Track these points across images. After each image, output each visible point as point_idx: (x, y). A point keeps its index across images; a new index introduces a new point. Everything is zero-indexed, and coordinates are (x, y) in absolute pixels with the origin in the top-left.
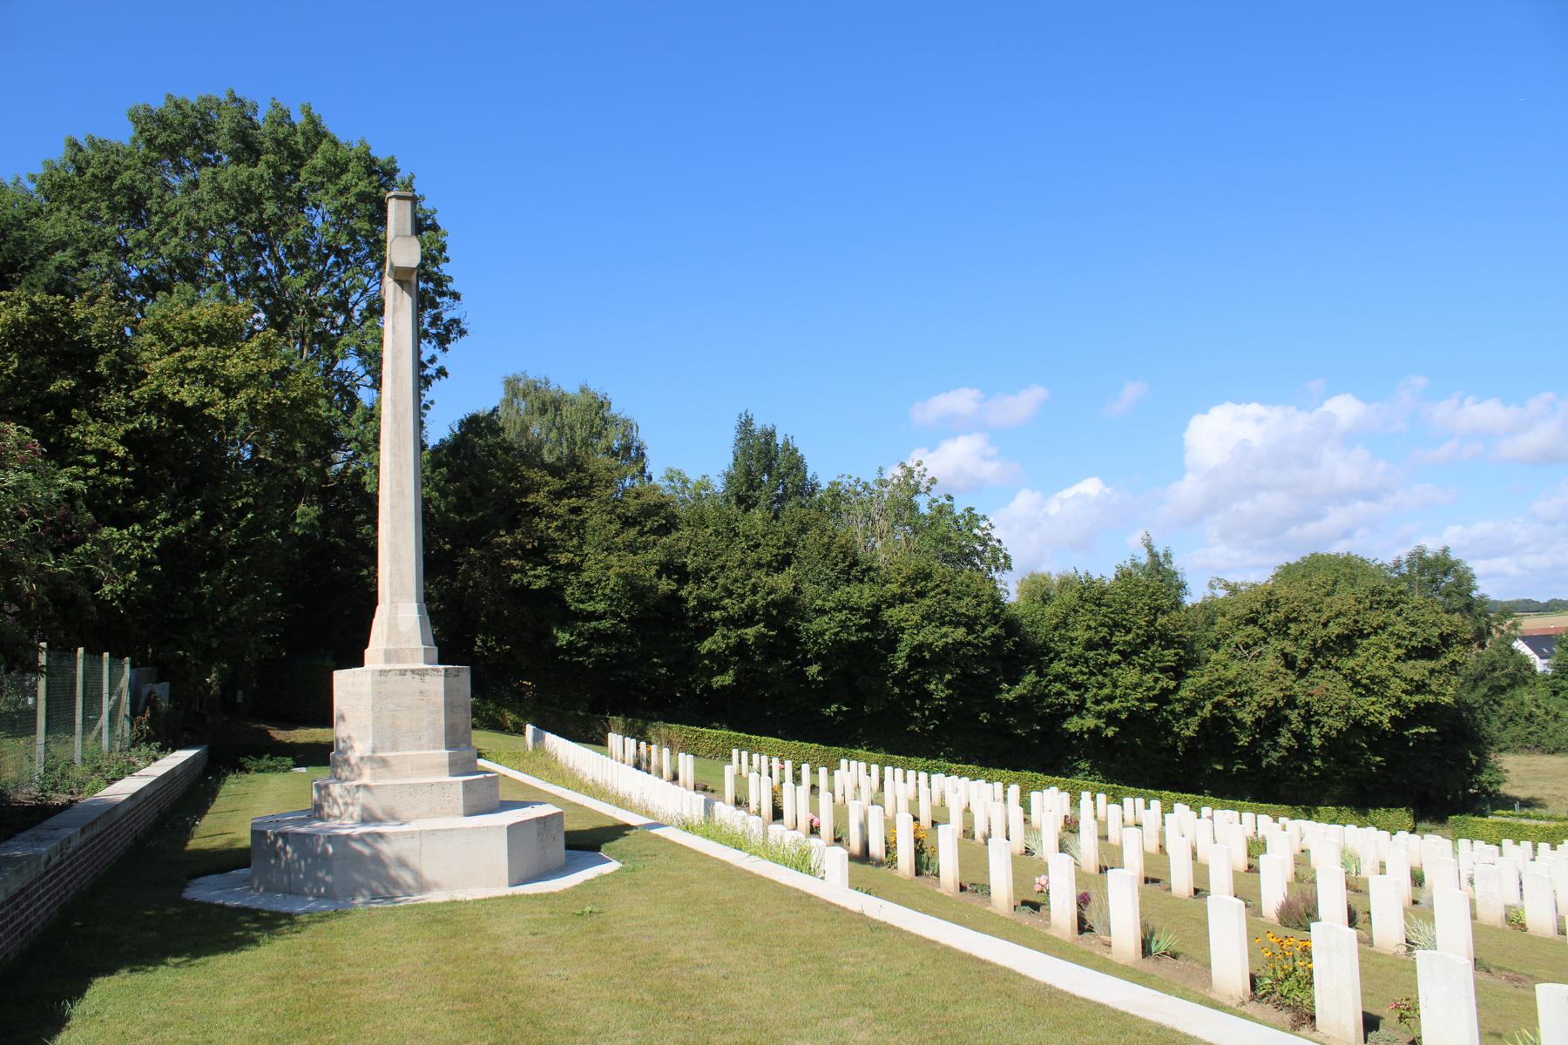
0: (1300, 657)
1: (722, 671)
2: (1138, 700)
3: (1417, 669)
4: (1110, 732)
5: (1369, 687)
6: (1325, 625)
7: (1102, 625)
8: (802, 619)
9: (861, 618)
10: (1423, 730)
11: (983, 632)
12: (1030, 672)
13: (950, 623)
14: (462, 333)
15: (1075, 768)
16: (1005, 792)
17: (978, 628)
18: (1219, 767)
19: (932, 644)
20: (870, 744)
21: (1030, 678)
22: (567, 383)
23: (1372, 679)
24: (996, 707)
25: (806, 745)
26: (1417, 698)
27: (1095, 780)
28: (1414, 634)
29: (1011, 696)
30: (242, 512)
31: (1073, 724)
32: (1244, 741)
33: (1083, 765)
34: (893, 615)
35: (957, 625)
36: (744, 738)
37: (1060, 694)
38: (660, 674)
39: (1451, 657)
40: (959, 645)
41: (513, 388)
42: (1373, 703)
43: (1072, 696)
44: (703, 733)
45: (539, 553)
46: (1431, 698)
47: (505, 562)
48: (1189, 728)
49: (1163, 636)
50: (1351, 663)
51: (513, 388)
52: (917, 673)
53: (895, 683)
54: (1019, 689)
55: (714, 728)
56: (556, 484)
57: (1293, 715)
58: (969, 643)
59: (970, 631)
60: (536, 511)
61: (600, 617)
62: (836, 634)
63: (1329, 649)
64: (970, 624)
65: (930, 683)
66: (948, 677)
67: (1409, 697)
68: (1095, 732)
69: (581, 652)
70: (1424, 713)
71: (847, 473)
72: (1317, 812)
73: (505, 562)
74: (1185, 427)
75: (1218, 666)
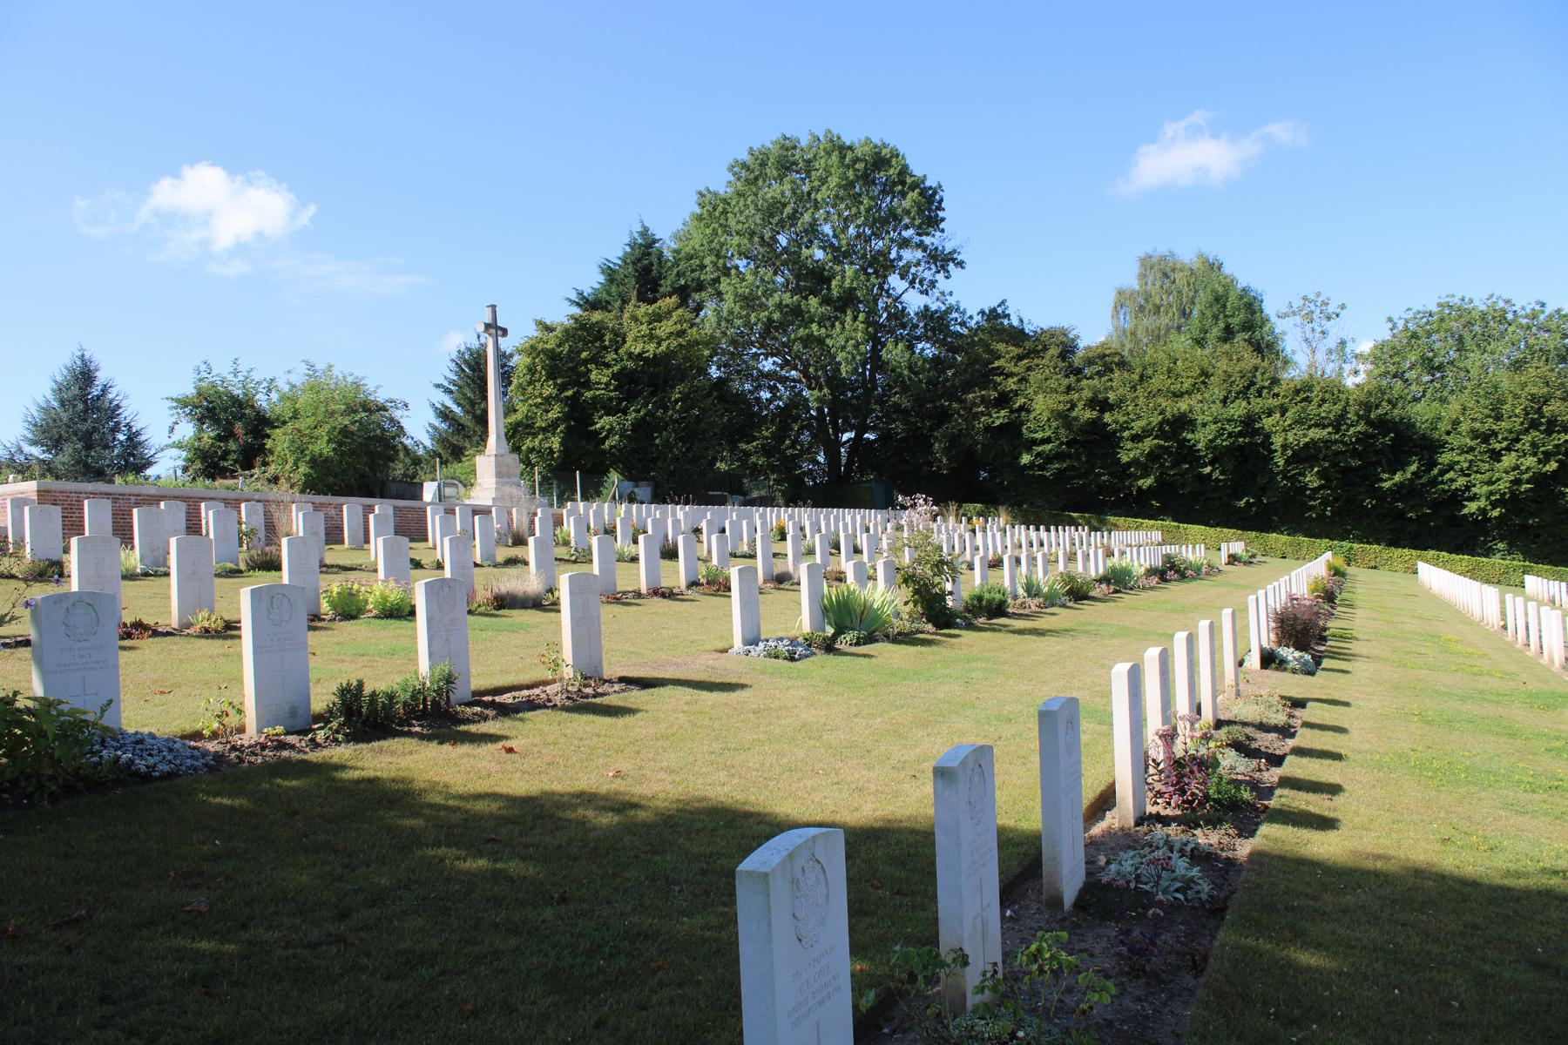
14: (960, 264)
22: (1187, 255)
25: (1225, 530)
27: (1514, 559)
30: (676, 401)
33: (1501, 546)
37: (1452, 480)
38: (1105, 481)
40: (1327, 443)
41: (1147, 264)
44: (1142, 523)
45: (1004, 400)
47: (975, 410)
51: (1147, 264)
54: (1398, 477)
56: (1015, 351)
59: (1337, 431)
60: (1000, 371)
61: (1047, 441)
64: (1338, 423)
68: (1483, 511)
69: (1041, 467)
73: (975, 410)
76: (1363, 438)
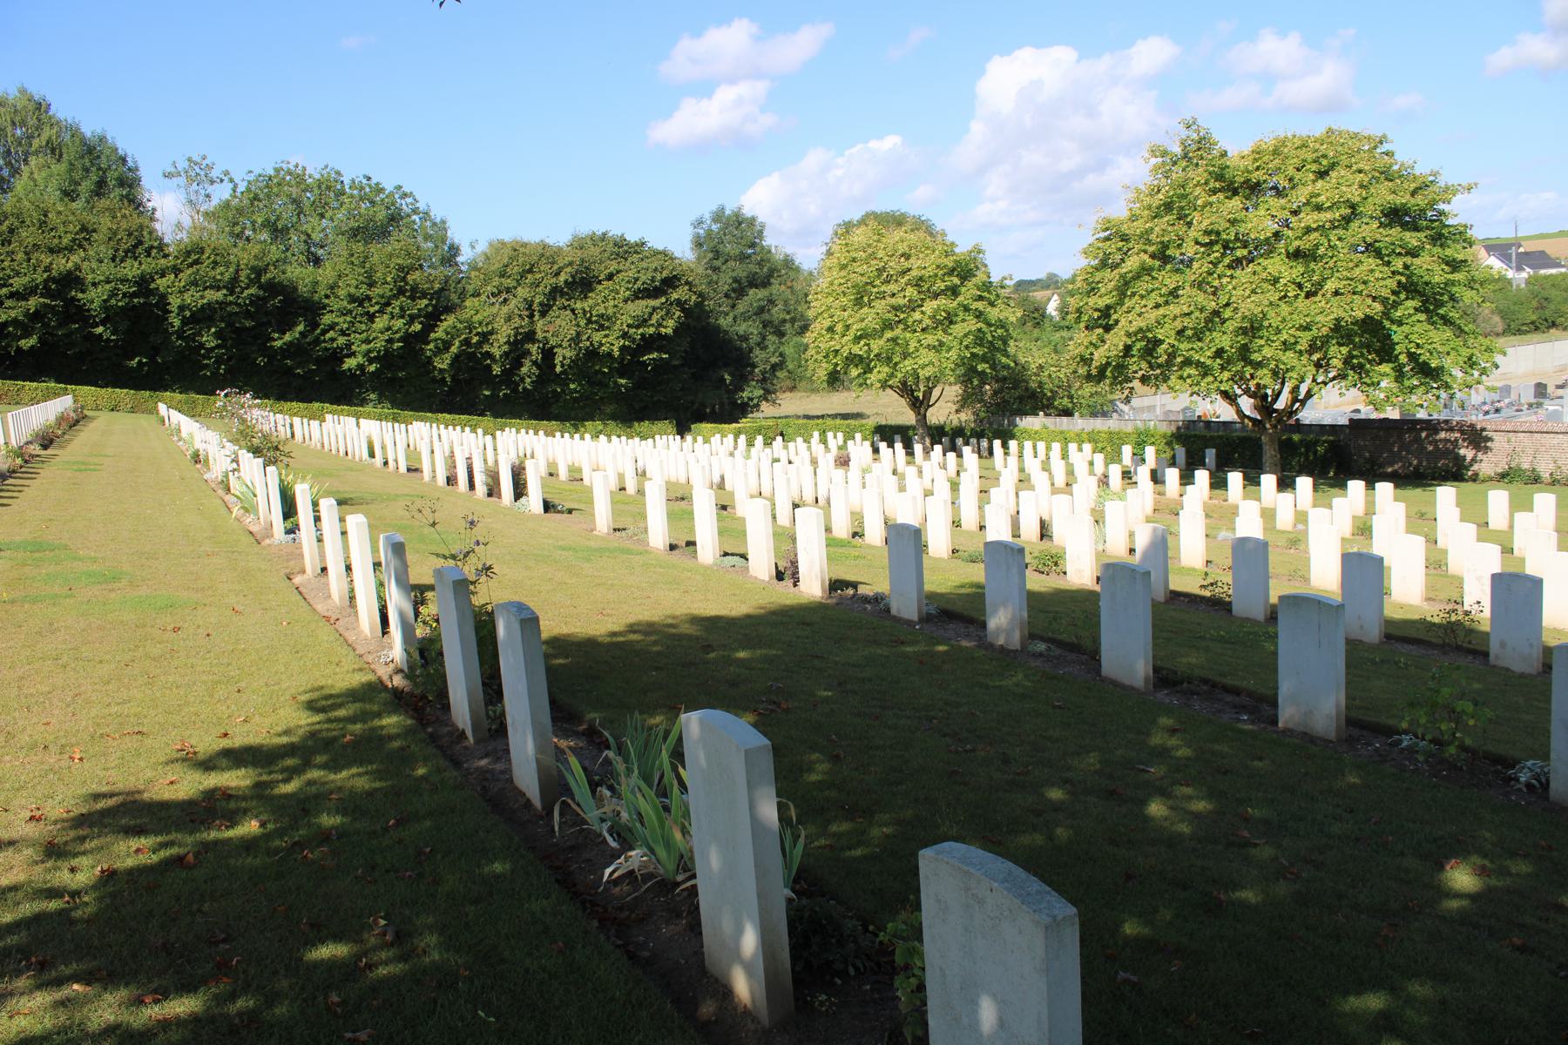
0: (537, 301)
1: (27, 335)
2: (386, 341)
3: (640, 307)
4: (372, 368)
5: (603, 323)
6: (557, 274)
7: (362, 283)
8: (83, 291)
9: (129, 287)
10: (655, 355)
11: (242, 293)
12: (300, 322)
13: (211, 287)
15: (364, 399)
16: (736, 441)
17: (238, 290)
18: (487, 393)
19: (190, 305)
20: (181, 387)
21: (301, 328)
23: (602, 316)
24: (271, 354)
25: (117, 390)
26: (640, 331)
28: (637, 280)
29: (278, 344)
31: (350, 363)
32: (497, 370)
33: (373, 396)
34: (162, 283)
35: (219, 289)
36: (61, 388)
37: (333, 340)
39: (675, 296)
42: (606, 336)
43: (341, 340)
44: (24, 386)
46: (652, 330)
48: (443, 363)
49: (414, 289)
50: (579, 305)
52: (191, 329)
53: (178, 339)
54: (288, 337)
55: (44, 382)
57: (534, 348)
58: (231, 303)
59: (232, 292)
62: (104, 301)
63: (563, 294)
65: (203, 336)
66: (213, 330)
67: (634, 330)
68: (361, 367)
70: (649, 343)
71: (286, 159)
72: (584, 426)
74: (981, 72)
75: (476, 310)
76: (255, 300)
